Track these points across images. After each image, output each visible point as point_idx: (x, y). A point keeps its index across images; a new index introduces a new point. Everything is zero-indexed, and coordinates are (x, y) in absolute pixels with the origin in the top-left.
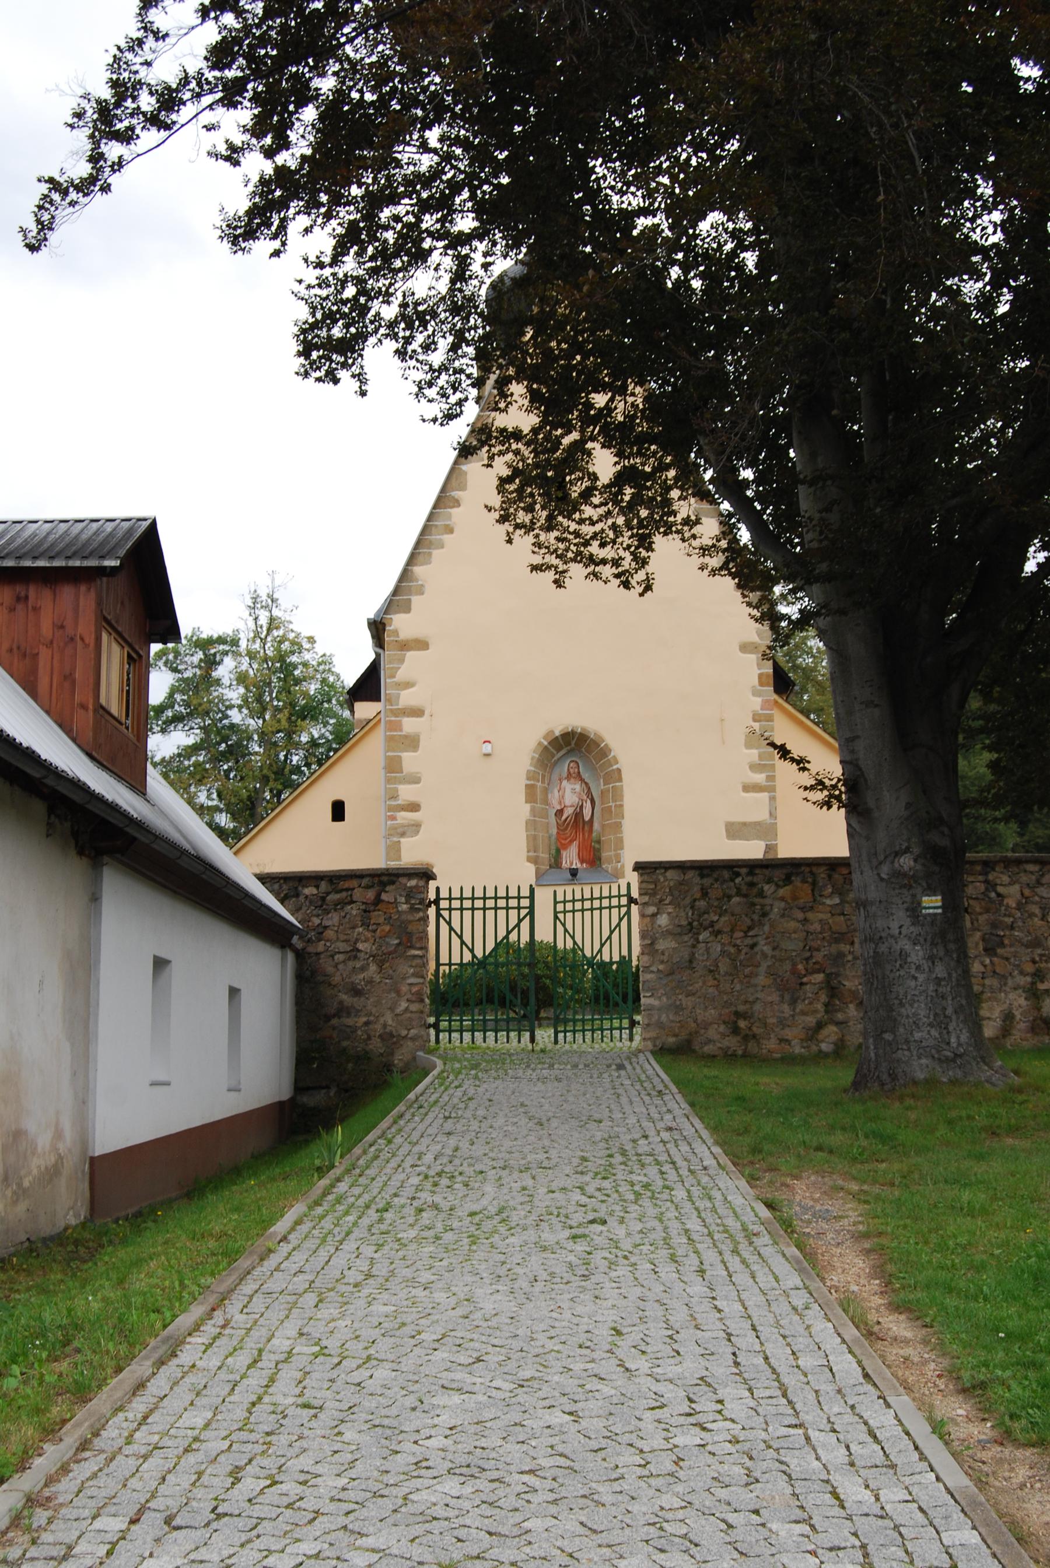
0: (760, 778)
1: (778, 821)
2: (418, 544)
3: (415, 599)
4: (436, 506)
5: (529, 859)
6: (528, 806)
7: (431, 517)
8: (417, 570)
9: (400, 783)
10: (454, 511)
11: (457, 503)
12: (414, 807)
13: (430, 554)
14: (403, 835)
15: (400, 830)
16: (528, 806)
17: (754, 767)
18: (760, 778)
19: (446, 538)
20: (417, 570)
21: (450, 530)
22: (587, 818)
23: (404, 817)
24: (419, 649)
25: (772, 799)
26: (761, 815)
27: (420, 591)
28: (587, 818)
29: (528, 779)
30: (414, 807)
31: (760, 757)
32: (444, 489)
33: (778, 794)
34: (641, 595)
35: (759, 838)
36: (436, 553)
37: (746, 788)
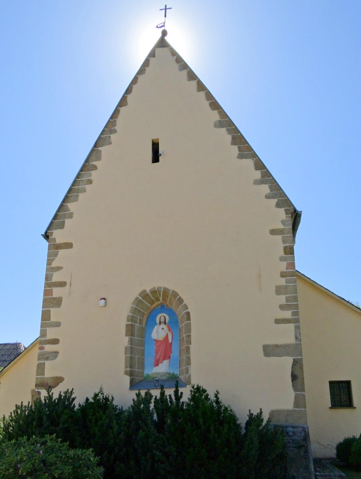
0: (288, 314)
1: (302, 342)
2: (70, 190)
3: (68, 222)
4: (81, 170)
5: (126, 373)
6: (127, 338)
7: (78, 176)
8: (71, 206)
9: (48, 327)
10: (93, 172)
11: (95, 168)
12: (55, 341)
13: (78, 196)
14: (47, 359)
15: (46, 356)
16: (127, 338)
17: (282, 307)
18: (288, 314)
19: (88, 187)
20: (71, 206)
21: (90, 182)
22: (170, 342)
23: (49, 348)
24: (67, 248)
25: (297, 328)
26: (291, 340)
27: (71, 216)
28: (170, 342)
29: (128, 321)
30: (55, 341)
31: (287, 300)
32: (87, 161)
33: (301, 325)
34: (60, 392)
35: (288, 355)
36: (81, 196)
37: (278, 321)
